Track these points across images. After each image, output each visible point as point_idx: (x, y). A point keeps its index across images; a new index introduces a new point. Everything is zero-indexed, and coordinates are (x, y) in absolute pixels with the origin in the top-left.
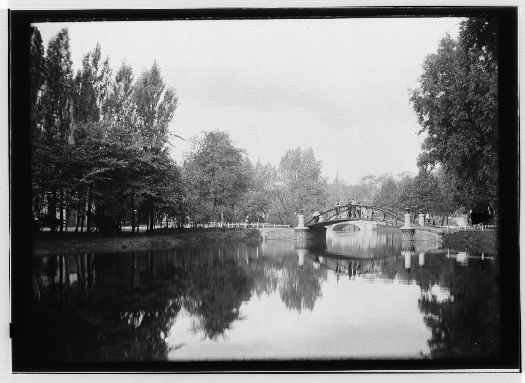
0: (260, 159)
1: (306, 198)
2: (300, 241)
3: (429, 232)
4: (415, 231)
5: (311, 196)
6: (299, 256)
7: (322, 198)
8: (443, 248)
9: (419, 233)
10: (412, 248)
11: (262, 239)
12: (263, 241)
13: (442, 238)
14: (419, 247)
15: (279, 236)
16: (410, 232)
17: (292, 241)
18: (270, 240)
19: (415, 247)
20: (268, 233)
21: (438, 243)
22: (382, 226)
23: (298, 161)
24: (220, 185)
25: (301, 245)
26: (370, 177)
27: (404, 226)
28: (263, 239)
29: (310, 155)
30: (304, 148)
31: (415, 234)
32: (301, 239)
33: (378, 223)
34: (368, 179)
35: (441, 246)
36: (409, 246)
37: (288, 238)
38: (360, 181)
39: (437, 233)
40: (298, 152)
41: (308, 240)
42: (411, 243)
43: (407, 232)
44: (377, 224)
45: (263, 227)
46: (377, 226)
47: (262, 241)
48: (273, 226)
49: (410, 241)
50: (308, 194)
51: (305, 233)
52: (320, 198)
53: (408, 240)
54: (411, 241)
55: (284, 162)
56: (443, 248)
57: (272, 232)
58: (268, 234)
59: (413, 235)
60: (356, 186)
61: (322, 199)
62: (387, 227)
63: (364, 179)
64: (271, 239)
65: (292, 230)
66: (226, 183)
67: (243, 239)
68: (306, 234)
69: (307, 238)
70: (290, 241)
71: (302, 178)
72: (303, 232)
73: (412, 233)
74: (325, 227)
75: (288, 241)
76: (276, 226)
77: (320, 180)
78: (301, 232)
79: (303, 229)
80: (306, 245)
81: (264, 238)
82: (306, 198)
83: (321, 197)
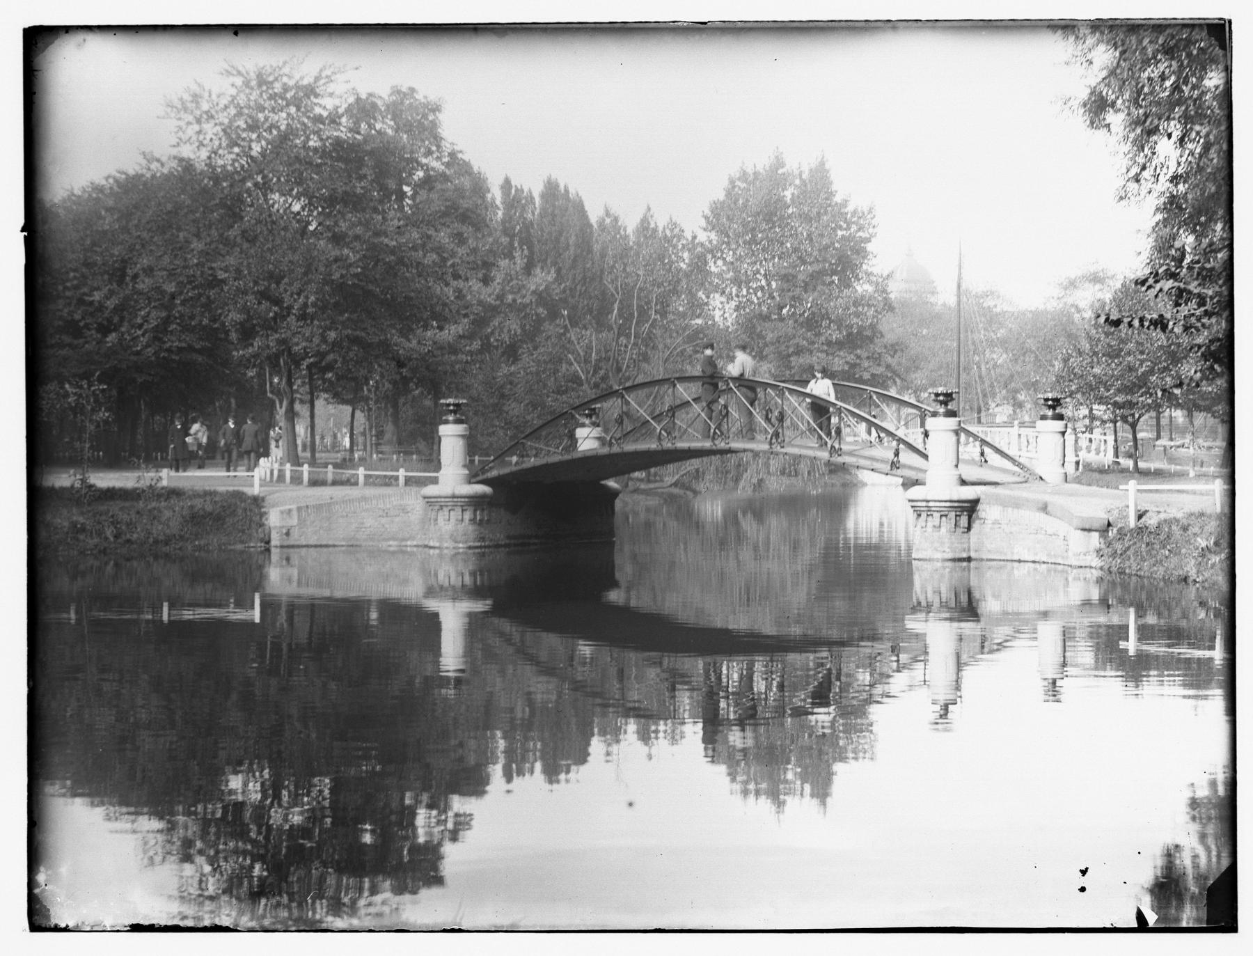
0: (649, 209)
1: (801, 360)
2: (441, 556)
3: (1043, 515)
4: (980, 507)
5: (825, 348)
6: (444, 626)
7: (868, 358)
8: (1105, 603)
9: (996, 522)
10: (964, 599)
11: (268, 542)
12: (273, 550)
13: (1098, 552)
14: (996, 596)
15: (353, 526)
16: (952, 514)
17: (412, 554)
18: (307, 546)
19: (976, 595)
20: (295, 513)
21: (1077, 579)
22: (1092, 470)
23: (772, 213)
24: (264, 295)
25: (448, 573)
26: (1096, 279)
27: (435, 481)
28: (273, 543)
29: (818, 183)
30: (799, 162)
31: (976, 526)
32: (448, 544)
33: (1081, 458)
34: (1087, 285)
35: (1095, 595)
36: (943, 590)
37: (394, 539)
38: (1058, 292)
39: (1076, 522)
40: (776, 176)
41: (483, 550)
42: (957, 575)
43: (937, 515)
44: (1075, 459)
45: (361, 479)
46: (1077, 469)
47: (268, 550)
48: (397, 478)
49: (949, 564)
50: (813, 343)
51: (468, 515)
52: (858, 357)
53: (939, 556)
54: (954, 560)
55: (718, 217)
56: (1105, 603)
57: (321, 506)
58: (294, 521)
59: (969, 528)
60: (1037, 314)
61: (866, 364)
62: (1114, 471)
63: (1072, 284)
64: (312, 542)
65: (413, 500)
66: (290, 284)
67: (156, 542)
68: (473, 520)
69: (482, 539)
70: (403, 552)
71: (788, 281)
72: (459, 510)
73: (964, 521)
74: (603, 482)
75: (393, 553)
76: (367, 477)
77: (863, 288)
78: (446, 510)
79: (454, 497)
80: (473, 574)
81: (275, 541)
82: (801, 360)
83: (865, 355)
